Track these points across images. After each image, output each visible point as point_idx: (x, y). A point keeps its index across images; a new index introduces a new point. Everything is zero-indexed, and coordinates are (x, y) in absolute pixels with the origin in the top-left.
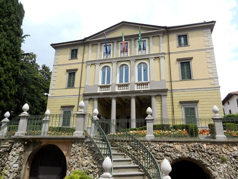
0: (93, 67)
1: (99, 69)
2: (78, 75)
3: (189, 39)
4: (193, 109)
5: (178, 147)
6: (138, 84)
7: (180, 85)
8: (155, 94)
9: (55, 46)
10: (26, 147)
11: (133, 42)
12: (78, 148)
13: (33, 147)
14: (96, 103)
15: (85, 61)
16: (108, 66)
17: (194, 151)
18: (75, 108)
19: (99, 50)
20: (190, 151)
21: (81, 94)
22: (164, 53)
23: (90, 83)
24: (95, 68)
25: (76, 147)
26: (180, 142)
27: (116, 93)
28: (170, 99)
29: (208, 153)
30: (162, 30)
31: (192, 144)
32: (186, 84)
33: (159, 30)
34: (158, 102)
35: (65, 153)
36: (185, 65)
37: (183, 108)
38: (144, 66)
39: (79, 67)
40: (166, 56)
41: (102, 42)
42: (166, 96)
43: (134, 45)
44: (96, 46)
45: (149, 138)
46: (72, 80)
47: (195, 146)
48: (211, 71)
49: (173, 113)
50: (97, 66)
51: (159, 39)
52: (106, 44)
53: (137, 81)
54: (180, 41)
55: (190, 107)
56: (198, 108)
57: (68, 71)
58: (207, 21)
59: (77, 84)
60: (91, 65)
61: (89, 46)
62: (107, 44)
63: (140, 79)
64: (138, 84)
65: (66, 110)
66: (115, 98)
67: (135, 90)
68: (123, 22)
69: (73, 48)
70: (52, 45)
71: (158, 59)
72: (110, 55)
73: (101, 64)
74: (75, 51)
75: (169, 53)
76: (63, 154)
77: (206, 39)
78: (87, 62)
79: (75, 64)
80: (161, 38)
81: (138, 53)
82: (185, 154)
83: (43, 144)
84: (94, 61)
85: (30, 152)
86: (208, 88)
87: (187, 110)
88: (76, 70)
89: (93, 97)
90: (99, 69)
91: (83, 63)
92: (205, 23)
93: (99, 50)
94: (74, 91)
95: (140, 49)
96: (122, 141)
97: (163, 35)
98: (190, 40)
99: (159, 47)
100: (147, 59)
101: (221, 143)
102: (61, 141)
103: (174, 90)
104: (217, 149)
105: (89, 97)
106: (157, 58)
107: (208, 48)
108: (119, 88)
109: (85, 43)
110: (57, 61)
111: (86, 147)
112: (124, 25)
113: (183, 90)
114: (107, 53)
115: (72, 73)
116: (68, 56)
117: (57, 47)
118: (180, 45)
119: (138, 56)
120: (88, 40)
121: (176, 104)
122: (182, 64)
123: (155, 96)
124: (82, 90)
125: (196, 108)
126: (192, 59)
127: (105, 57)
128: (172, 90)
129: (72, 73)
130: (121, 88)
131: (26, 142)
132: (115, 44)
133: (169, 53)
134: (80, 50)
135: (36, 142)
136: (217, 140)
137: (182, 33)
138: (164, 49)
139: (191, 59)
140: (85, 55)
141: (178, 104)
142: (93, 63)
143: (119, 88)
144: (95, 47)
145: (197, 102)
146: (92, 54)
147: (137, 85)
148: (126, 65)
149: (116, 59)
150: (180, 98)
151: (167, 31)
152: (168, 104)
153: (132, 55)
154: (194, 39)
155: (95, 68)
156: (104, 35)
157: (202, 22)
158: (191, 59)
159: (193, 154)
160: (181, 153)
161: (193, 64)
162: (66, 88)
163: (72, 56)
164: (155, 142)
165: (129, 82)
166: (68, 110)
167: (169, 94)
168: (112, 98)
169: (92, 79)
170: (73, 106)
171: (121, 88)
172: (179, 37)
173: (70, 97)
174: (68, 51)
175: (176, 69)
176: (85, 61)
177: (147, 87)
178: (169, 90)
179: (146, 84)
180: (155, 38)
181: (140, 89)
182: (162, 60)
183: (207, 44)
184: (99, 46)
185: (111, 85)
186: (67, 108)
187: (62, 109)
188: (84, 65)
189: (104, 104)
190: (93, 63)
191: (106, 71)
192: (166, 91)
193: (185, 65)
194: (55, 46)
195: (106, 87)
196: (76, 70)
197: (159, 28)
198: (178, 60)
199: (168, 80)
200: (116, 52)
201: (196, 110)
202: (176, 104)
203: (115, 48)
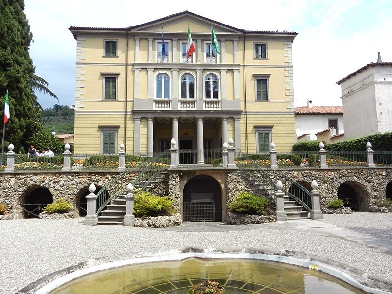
0: (144, 72)
1: (153, 75)
2: (120, 82)
3: (268, 51)
4: (113, 135)
5: (295, 174)
6: (157, 102)
7: (255, 107)
8: (228, 116)
9: (77, 31)
10: (181, 178)
11: (175, 43)
12: (234, 177)
13: (188, 177)
14: (151, 123)
15: (131, 61)
16: (214, 75)
17: (307, 176)
18: (120, 129)
19: (151, 48)
20: (303, 176)
21: (129, 109)
22: (239, 66)
23: (140, 95)
24: (147, 74)
25: (232, 176)
26: (297, 170)
27: (179, 112)
28: (243, 122)
29: (316, 177)
30: (239, 33)
31: (305, 172)
32: (262, 106)
33: (235, 33)
34: (229, 126)
35: (219, 181)
36: (262, 81)
37: (257, 134)
38: (165, 79)
39: (121, 70)
40: (241, 69)
41: (156, 37)
42: (240, 118)
43: (200, 49)
44: (231, 42)
45: (120, 170)
46: (111, 89)
47: (307, 173)
48: (288, 93)
49: (247, 139)
50: (150, 72)
51: (147, 43)
52: (163, 41)
53: (180, 98)
54: (257, 52)
55: (264, 132)
56: (118, 135)
57: (103, 74)
58: (280, 31)
59: (120, 95)
60: (154, 70)
61: (135, 39)
62: (165, 41)
63: (159, 95)
64: (157, 102)
65: (107, 132)
66: (151, 118)
67: (179, 109)
68: (187, 12)
69: (111, 39)
70: (71, 29)
71: (230, 71)
72: (168, 58)
73: (206, 71)
74: (111, 44)
75: (245, 66)
76: (218, 182)
77: (286, 53)
78: (134, 65)
79: (113, 65)
80: (236, 44)
81: (206, 61)
82: (300, 178)
83: (198, 174)
84: (145, 64)
85: (185, 182)
86: (283, 112)
87: (106, 136)
88: (118, 74)
89: (147, 116)
90: (153, 75)
91: (127, 64)
92: (277, 33)
93: (151, 48)
94: (118, 106)
95: (208, 55)
96: (252, 171)
97: (238, 41)
98: (270, 52)
99: (232, 56)
100: (194, 71)
101: (324, 170)
102: (216, 172)
103: (249, 112)
104: (321, 175)
105: (140, 115)
106: (231, 70)
107: (287, 65)
108: (182, 106)
109: (129, 34)
110: (83, 56)
111: (239, 176)
112: (187, 16)
113: (258, 113)
114: (164, 53)
115: (110, 79)
116: (102, 51)
117: (77, 32)
118: (257, 58)
119: (206, 65)
120: (134, 31)
121: (250, 128)
122: (259, 81)
123: (227, 118)
124: (130, 105)
125: (270, 133)
126: (119, 75)
127: (160, 59)
128: (246, 112)
129: (110, 79)
130: (185, 105)
131: (181, 174)
132: (175, 43)
133: (245, 66)
134: (121, 44)
135: (191, 173)
136: (322, 168)
137: (261, 41)
138: (239, 61)
139: (268, 76)
140: (131, 53)
141: (252, 129)
142: (144, 67)
143: (182, 106)
144: (144, 42)
145: (271, 127)
146: (140, 54)
147: (156, 103)
148: (191, 75)
149: (177, 64)
150: (99, 122)
151: (244, 36)
152: (242, 129)
153: (199, 63)
154: (274, 52)
155: (147, 74)
156: (158, 26)
157: (275, 31)
158: (268, 76)
159: (306, 178)
160: (298, 178)
161: (271, 82)
162: (103, 101)
163: (107, 52)
164: (279, 170)
165: (171, 99)
166: (110, 132)
167: (242, 116)
168: (174, 118)
169: (142, 90)
170: (118, 127)
171: (185, 105)
172: (257, 45)
173: (113, 113)
174: (101, 42)
175: (252, 86)
176: (131, 61)
177: (168, 106)
178: (244, 112)
179: (168, 103)
180: (228, 43)
181: (209, 109)
182: (236, 73)
183: (286, 59)
184: (151, 42)
185: (172, 101)
186: (108, 129)
187: (254, 129)
188: (130, 68)
189: (162, 127)
190: (144, 67)
191: (163, 80)
192: (239, 112)
193: (262, 81)
194: (77, 31)
195: (213, 103)
196: (118, 74)
197: (236, 31)
198: (254, 76)
199: (242, 100)
200: (176, 56)
201: (270, 135)
202: (250, 128)
203: (175, 49)
